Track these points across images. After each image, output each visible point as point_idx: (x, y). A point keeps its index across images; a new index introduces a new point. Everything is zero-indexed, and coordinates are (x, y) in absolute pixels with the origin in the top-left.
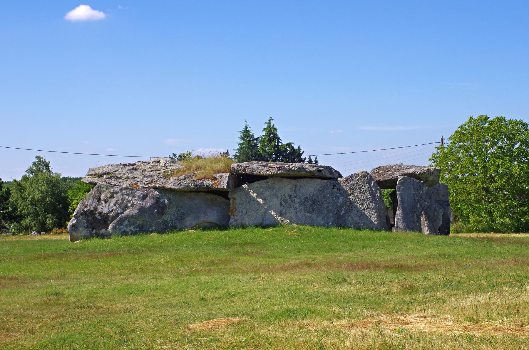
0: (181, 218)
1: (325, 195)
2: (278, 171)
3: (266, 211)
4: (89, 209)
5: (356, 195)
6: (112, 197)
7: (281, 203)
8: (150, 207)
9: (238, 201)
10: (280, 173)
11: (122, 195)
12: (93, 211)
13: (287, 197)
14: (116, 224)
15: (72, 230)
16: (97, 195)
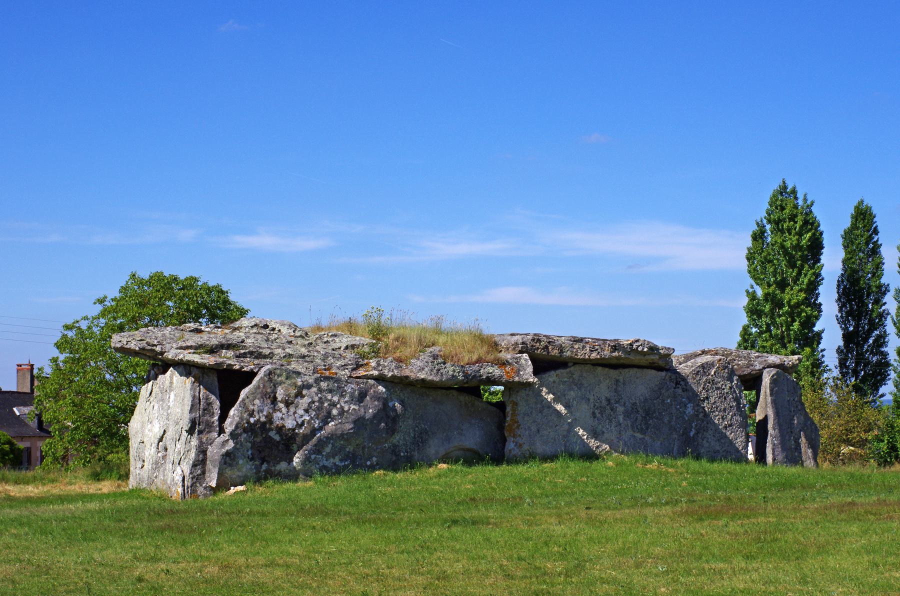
0: (420, 440)
1: (663, 401)
2: (612, 352)
3: (571, 426)
4: (258, 420)
5: (712, 400)
6: (299, 395)
7: (594, 413)
8: (375, 416)
9: (522, 408)
10: (616, 358)
11: (320, 390)
12: (264, 424)
13: (604, 403)
14: (311, 452)
15: (225, 463)
16: (269, 390)
